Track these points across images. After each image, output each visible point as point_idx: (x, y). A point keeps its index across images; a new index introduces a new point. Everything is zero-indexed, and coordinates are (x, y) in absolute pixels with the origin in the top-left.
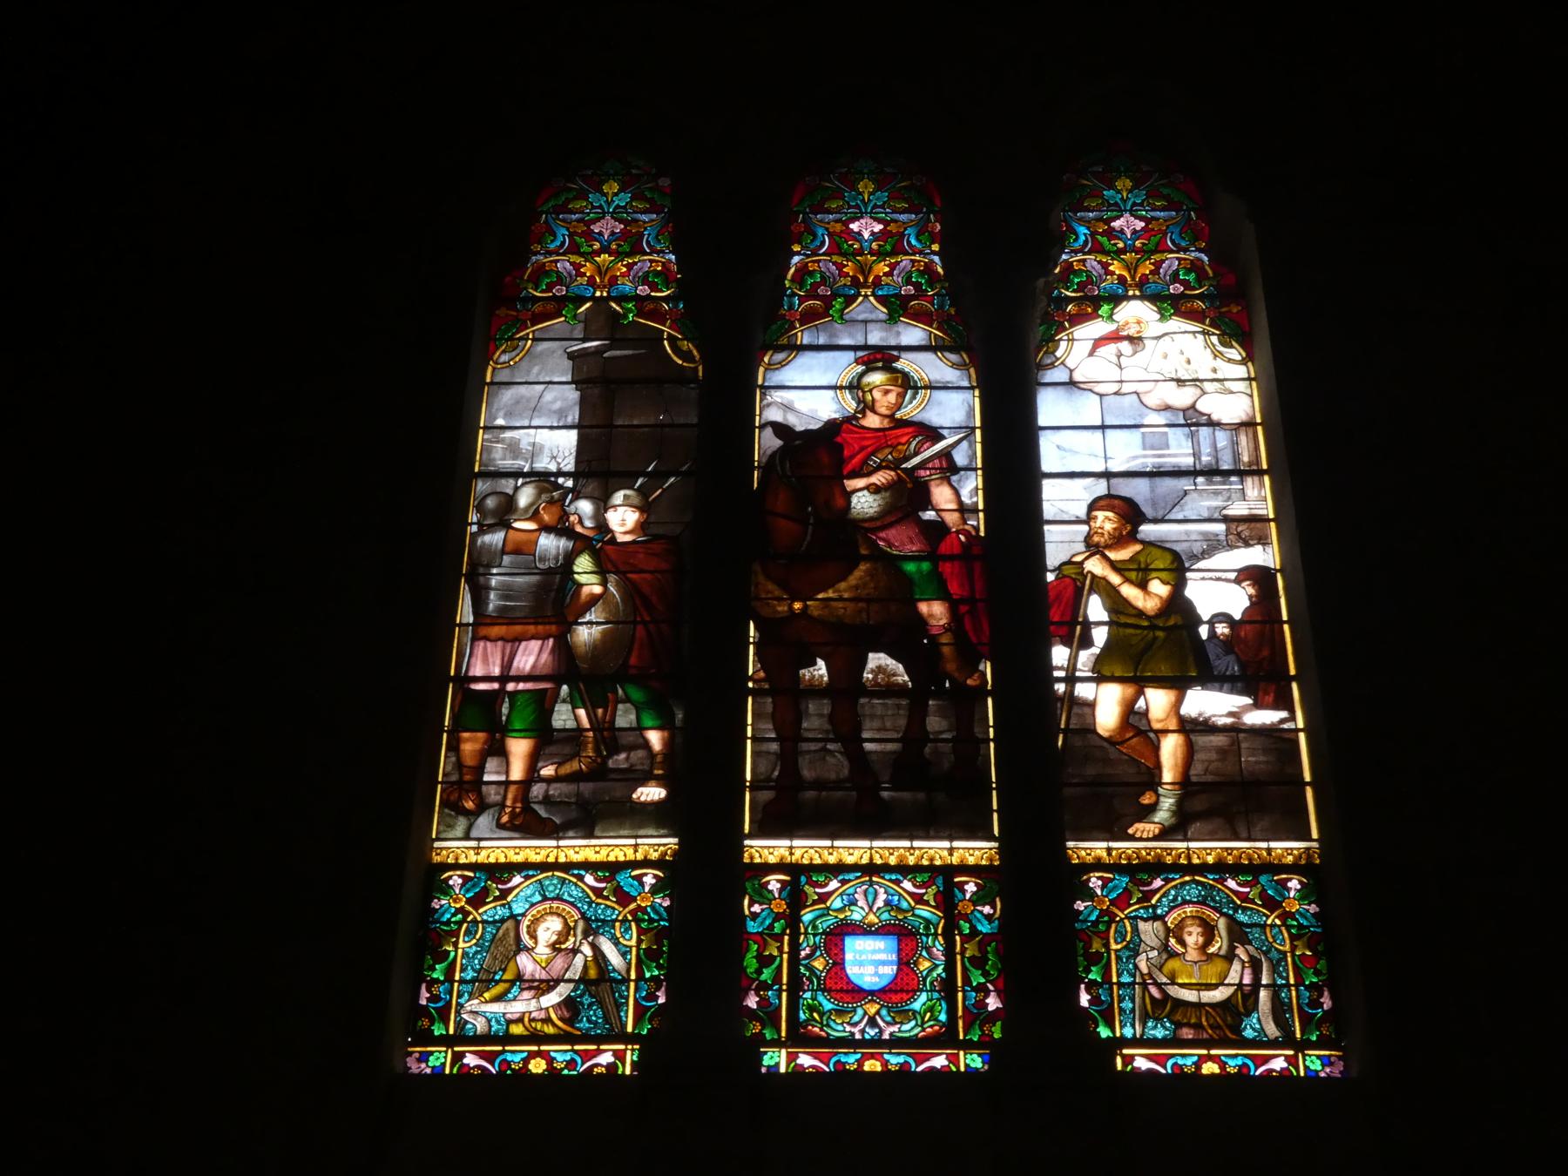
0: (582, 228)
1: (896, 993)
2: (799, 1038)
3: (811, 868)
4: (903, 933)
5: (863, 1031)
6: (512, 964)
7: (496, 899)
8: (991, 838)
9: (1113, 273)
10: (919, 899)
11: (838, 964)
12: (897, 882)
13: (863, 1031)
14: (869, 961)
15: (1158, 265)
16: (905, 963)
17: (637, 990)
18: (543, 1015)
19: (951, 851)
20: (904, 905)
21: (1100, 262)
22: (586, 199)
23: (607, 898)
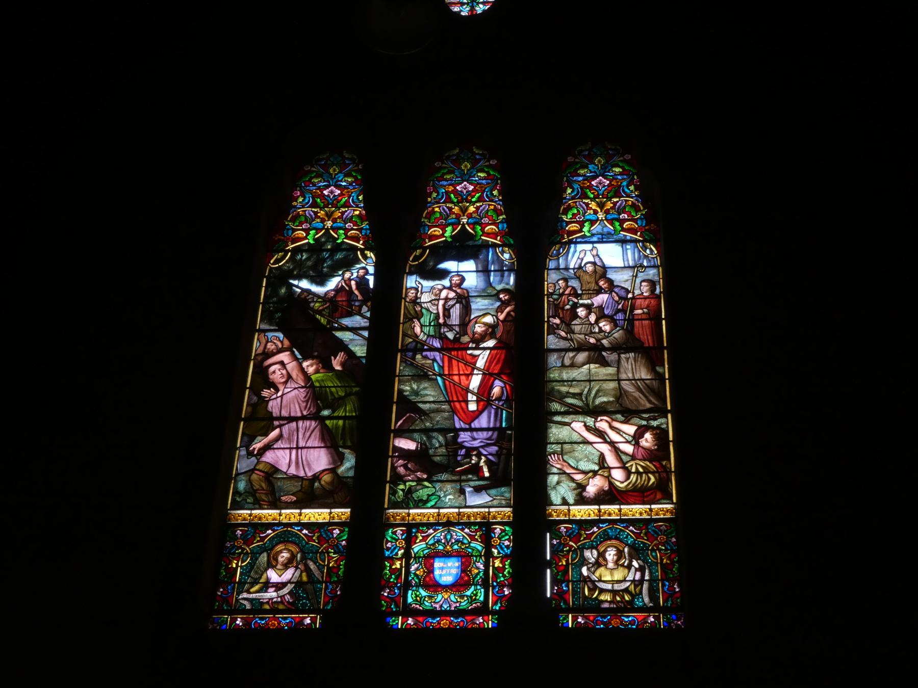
0: (451, 189)
1: (459, 586)
2: (407, 611)
3: (417, 525)
4: (465, 558)
5: (441, 606)
6: (265, 575)
7: (421, 541)
8: (673, 503)
9: (591, 209)
10: (473, 538)
11: (431, 570)
12: (462, 530)
13: (441, 606)
14: (446, 571)
15: (343, 213)
16: (465, 568)
17: (663, 585)
18: (279, 599)
19: (280, 515)
20: (465, 541)
21: (448, 207)
22: (587, 168)
23: (642, 538)
